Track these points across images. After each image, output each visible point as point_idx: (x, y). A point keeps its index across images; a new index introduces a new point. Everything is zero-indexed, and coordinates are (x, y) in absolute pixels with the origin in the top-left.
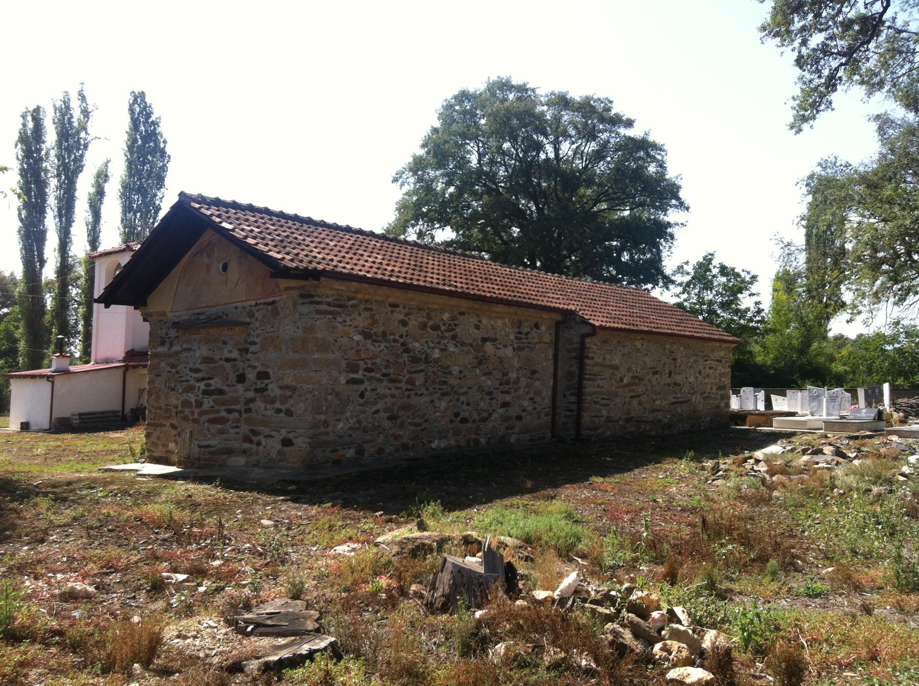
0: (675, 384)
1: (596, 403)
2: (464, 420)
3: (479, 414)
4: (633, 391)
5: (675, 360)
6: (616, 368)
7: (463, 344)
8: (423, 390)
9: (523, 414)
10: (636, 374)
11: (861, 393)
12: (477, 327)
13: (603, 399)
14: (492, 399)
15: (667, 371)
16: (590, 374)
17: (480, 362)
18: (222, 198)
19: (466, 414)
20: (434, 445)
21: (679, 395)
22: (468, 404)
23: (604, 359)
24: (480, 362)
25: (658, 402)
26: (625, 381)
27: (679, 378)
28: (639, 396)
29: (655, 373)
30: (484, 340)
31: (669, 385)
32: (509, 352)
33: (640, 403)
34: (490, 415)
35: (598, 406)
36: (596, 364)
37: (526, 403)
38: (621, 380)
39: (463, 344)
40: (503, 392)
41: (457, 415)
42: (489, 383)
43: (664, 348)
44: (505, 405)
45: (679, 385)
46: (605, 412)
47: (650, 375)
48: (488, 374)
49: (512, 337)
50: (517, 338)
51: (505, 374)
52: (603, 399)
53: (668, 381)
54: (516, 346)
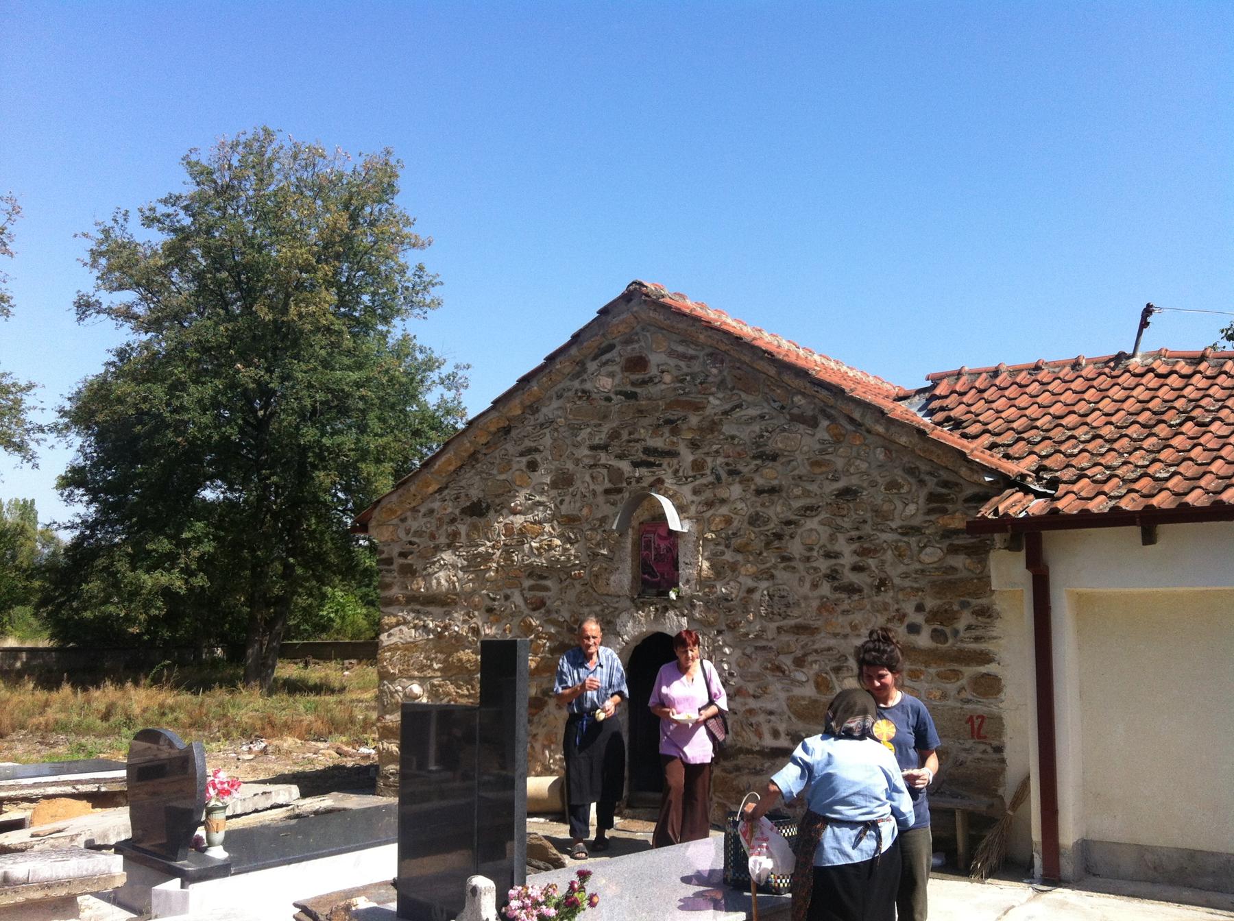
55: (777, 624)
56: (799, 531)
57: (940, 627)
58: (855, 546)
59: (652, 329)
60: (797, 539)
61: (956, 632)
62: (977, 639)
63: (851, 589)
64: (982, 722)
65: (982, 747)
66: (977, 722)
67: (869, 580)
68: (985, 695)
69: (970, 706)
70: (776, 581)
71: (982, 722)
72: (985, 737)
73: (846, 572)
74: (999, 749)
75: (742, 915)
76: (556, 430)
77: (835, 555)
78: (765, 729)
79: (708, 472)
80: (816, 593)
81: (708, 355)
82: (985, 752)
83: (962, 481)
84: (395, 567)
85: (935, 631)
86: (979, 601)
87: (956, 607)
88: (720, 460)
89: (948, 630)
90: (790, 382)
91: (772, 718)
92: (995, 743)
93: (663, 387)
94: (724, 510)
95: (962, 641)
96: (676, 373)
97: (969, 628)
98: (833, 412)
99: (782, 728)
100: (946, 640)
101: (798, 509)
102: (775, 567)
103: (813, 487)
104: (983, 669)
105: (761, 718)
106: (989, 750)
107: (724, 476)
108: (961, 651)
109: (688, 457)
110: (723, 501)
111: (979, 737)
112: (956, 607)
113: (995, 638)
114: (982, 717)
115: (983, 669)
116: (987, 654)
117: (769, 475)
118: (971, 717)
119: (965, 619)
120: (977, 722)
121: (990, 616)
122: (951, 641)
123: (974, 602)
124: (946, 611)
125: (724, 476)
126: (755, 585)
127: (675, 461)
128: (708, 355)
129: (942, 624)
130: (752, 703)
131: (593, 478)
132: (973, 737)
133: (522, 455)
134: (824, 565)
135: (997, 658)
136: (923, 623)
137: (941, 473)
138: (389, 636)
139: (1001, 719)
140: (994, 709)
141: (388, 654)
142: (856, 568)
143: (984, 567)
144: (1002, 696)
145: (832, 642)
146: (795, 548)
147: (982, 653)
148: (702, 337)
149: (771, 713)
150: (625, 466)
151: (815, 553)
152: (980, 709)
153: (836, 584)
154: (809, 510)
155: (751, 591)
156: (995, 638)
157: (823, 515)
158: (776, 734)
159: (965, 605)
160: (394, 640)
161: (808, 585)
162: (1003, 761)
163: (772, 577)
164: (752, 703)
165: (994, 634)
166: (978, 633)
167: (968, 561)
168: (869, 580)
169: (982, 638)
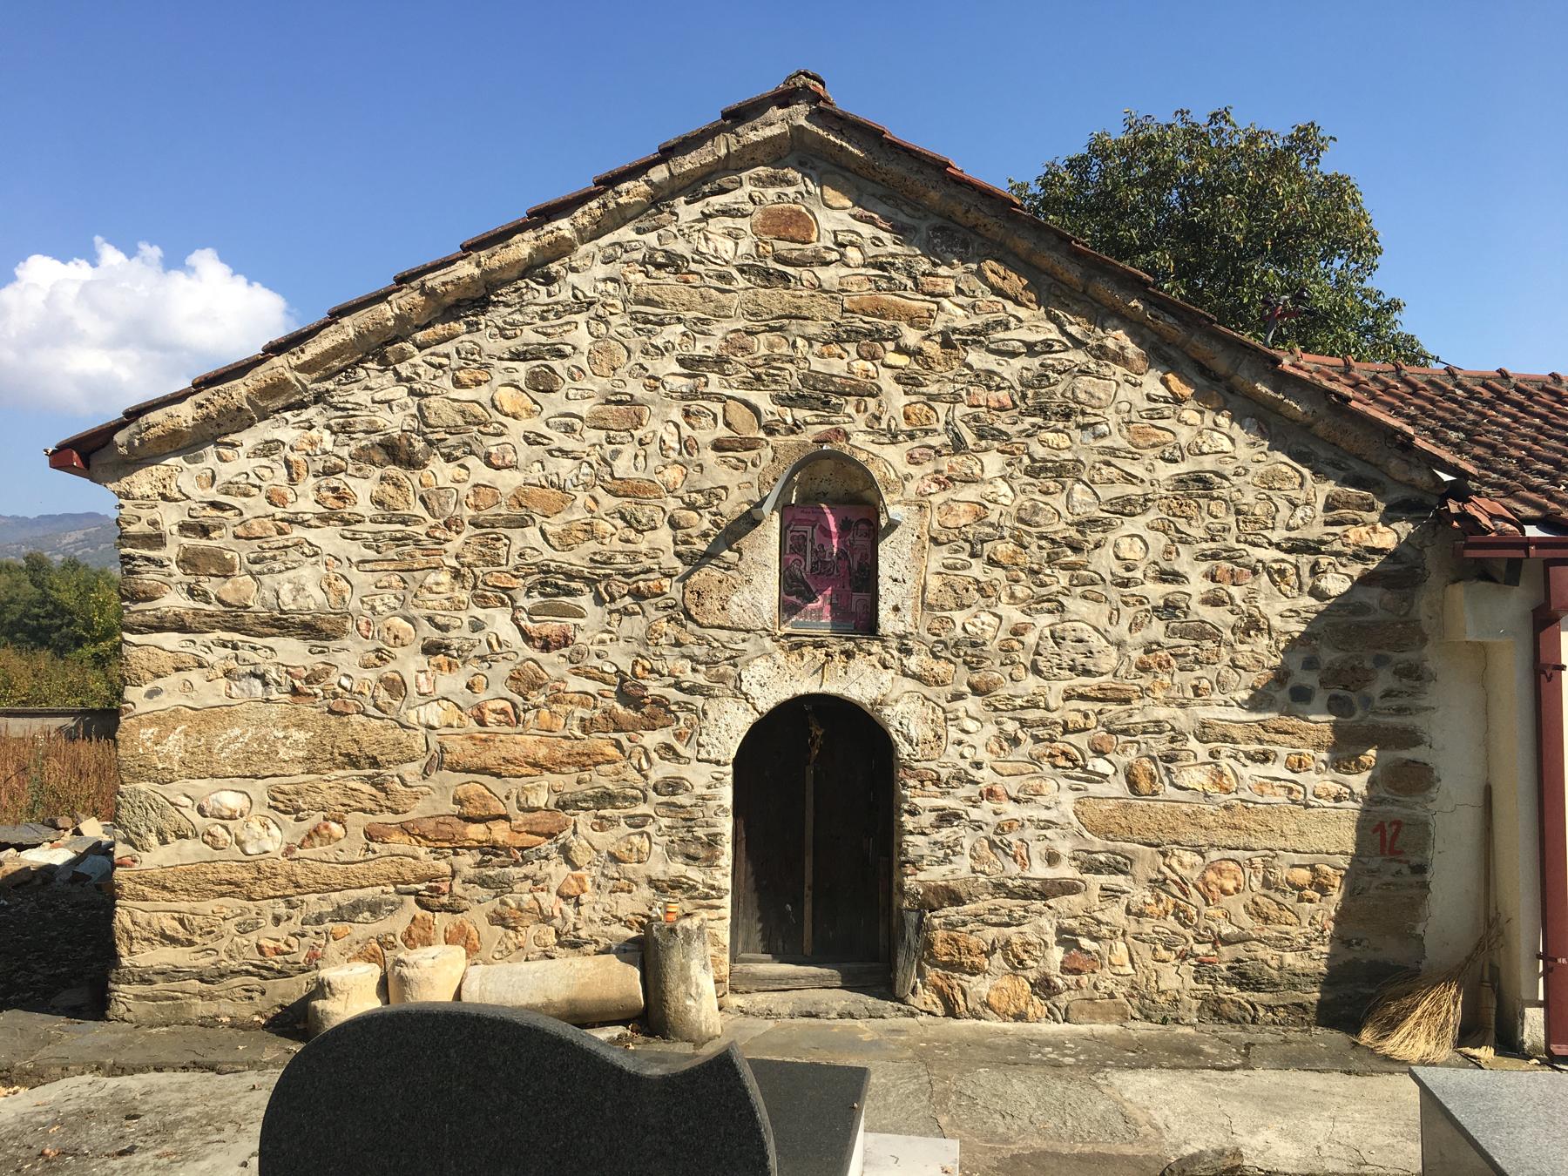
55: (1063, 685)
56: (1111, 537)
57: (1342, 693)
58: (1205, 566)
59: (823, 165)
60: (1108, 550)
61: (1368, 701)
62: (1400, 711)
63: (1202, 632)
64: (1397, 831)
65: (1395, 866)
66: (1390, 832)
67: (1231, 619)
68: (1409, 791)
69: (1383, 808)
70: (1067, 616)
71: (1397, 831)
72: (1401, 852)
73: (1194, 604)
74: (1420, 869)
75: (949, 1151)
76: (599, 318)
77: (1174, 577)
78: (1037, 849)
79: (940, 427)
80: (1139, 636)
81: (935, 229)
82: (1399, 872)
83: (1385, 479)
84: (170, 552)
85: (1334, 698)
86: (1403, 656)
87: (1368, 665)
88: (961, 409)
89: (1354, 697)
90: (339, 338)
91: (1048, 833)
92: (1415, 860)
93: (844, 271)
94: (970, 493)
95: (1375, 713)
96: (871, 251)
97: (1388, 694)
98: (1173, 353)
99: (1064, 848)
100: (1352, 713)
101: (1110, 502)
102: (1066, 592)
103: (1137, 470)
104: (1406, 755)
105: (1030, 832)
106: (1406, 870)
107: (969, 438)
108: (1375, 727)
109: (897, 400)
110: (969, 480)
111: (1392, 852)
112: (1368, 665)
113: (1426, 709)
114: (1398, 824)
115: (1406, 755)
116: (1413, 732)
117: (1056, 443)
118: (1382, 823)
119: (1384, 680)
120: (1390, 832)
121: (1419, 678)
122: (1359, 714)
123: (1397, 657)
124: (1353, 668)
125: (969, 438)
126: (1027, 619)
127: (872, 403)
128: (935, 229)
129: (1346, 687)
130: (1011, 810)
131: (687, 414)
132: (1382, 853)
133: (517, 356)
134: (1156, 592)
135: (1426, 739)
136: (1317, 685)
137: (1352, 464)
138: (151, 694)
139: (1426, 824)
140: (1419, 811)
141: (149, 733)
142: (1214, 601)
143: (1411, 606)
144: (1433, 792)
145: (1162, 713)
146: (1103, 562)
147: (1405, 730)
148: (933, 194)
149: (1049, 824)
150: (762, 399)
151: (1138, 574)
152: (1397, 812)
153: (1174, 624)
154: (1125, 508)
155: (1017, 632)
156: (1426, 709)
157: (1152, 516)
158: (1052, 859)
159: (1381, 661)
160: (165, 702)
161: (1125, 623)
162: (1425, 886)
163: (1062, 608)
164: (1011, 810)
165: (1424, 703)
166: (1403, 701)
167: (1388, 597)
168: (1231, 619)
169: (1405, 709)
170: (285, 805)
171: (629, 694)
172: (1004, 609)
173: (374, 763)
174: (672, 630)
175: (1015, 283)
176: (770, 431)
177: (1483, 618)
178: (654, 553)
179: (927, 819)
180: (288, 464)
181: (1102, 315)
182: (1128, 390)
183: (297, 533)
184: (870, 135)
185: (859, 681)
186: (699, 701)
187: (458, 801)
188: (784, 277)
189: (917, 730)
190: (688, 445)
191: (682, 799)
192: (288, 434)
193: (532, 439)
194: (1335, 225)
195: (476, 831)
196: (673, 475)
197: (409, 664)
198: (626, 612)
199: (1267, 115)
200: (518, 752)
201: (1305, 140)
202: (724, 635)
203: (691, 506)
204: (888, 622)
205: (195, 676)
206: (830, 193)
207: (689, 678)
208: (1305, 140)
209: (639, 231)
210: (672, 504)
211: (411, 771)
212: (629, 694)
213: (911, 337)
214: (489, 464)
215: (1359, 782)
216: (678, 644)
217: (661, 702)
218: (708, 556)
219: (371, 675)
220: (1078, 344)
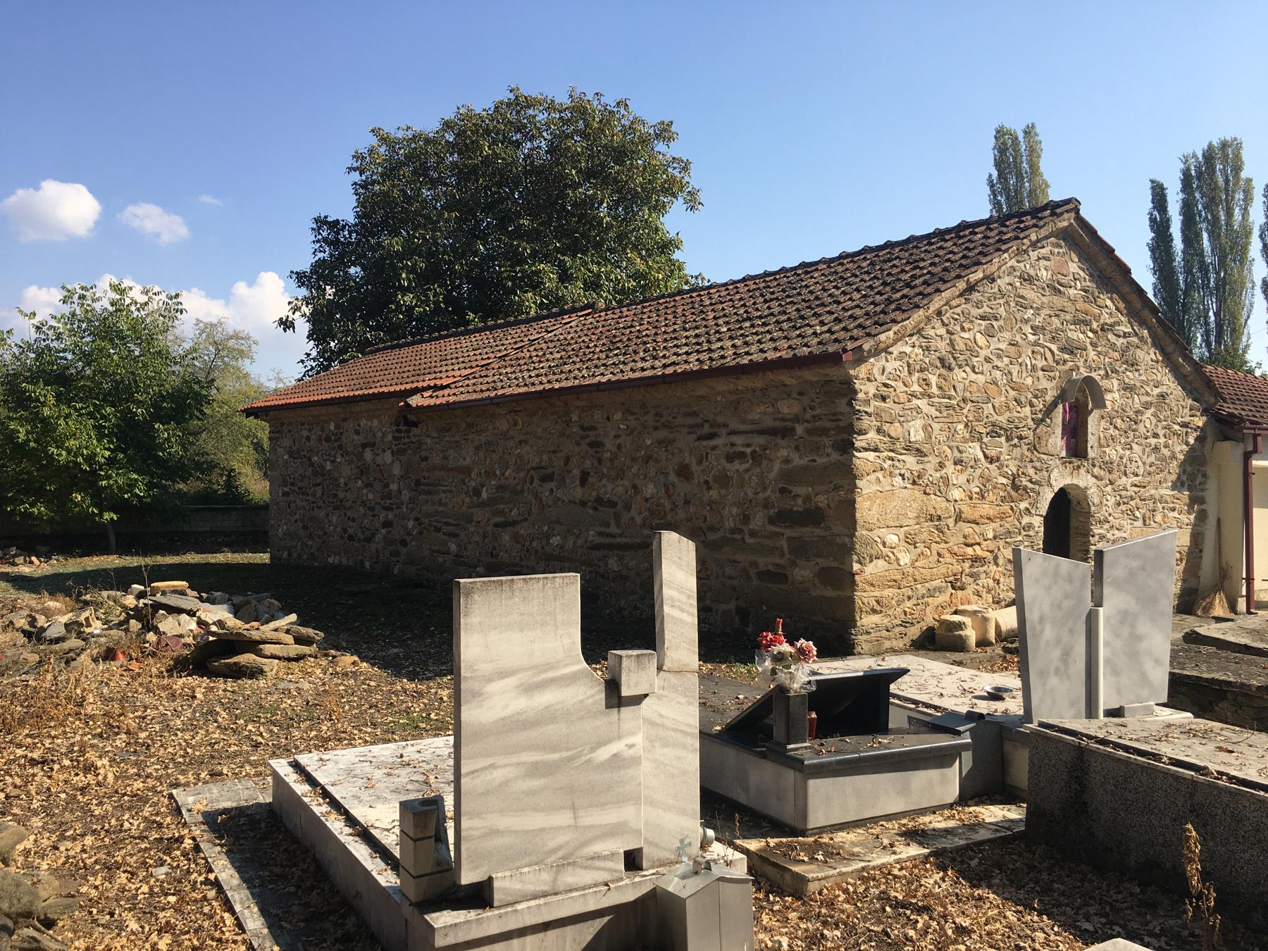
0: (599, 500)
1: (438, 530)
2: (351, 538)
3: (363, 533)
4: (501, 513)
5: (596, 445)
6: (466, 471)
7: (348, 453)
8: (321, 503)
9: (408, 538)
10: (503, 481)
11: (678, 569)
12: (357, 433)
13: (447, 524)
14: (374, 516)
15: (576, 472)
16: (427, 484)
17: (362, 473)
18: (873, 244)
19: (351, 531)
20: (331, 560)
21: (613, 529)
22: (353, 520)
23: (446, 458)
24: (362, 473)
25: (556, 540)
26: (484, 495)
27: (610, 489)
28: (514, 523)
29: (544, 479)
30: (364, 446)
31: (583, 504)
32: (388, 457)
33: (516, 537)
34: (373, 535)
35: (441, 535)
36: (434, 468)
37: (411, 524)
38: (477, 492)
39: (348, 453)
40: (386, 509)
41: (345, 531)
42: (371, 496)
43: (568, 423)
44: (387, 524)
45: (613, 504)
46: (453, 547)
47: (536, 483)
48: (369, 485)
49: (390, 438)
50: (395, 438)
51: (387, 486)
52: (447, 524)
53: (578, 493)
54: (395, 449)
74: (1201, 551)
170: (911, 541)
171: (1015, 487)
172: (1119, 448)
173: (939, 519)
174: (1028, 454)
175: (1122, 305)
176: (1058, 363)
177: (1230, 453)
178: (1025, 418)
179: (1097, 538)
180: (909, 365)
181: (1143, 323)
182: (1148, 355)
183: (915, 401)
184: (1092, 232)
185: (1083, 480)
186: (1037, 487)
187: (965, 537)
188: (1060, 291)
189: (1096, 501)
190: (1034, 368)
191: (1031, 533)
192: (908, 349)
193: (988, 360)
194: (667, 186)
195: (969, 550)
196: (1029, 381)
197: (950, 469)
198: (1015, 446)
199: (647, 111)
200: (984, 513)
201: (664, 132)
202: (1045, 457)
203: (1036, 397)
204: (1091, 454)
205: (880, 475)
206: (1073, 255)
207: (1035, 478)
208: (664, 132)
209: (1018, 262)
210: (1030, 396)
211: (951, 522)
212: (1015, 487)
213: (1095, 325)
214: (974, 371)
215: (1192, 517)
216: (1032, 461)
217: (1025, 489)
218: (1043, 420)
219: (938, 475)
220: (1136, 334)
